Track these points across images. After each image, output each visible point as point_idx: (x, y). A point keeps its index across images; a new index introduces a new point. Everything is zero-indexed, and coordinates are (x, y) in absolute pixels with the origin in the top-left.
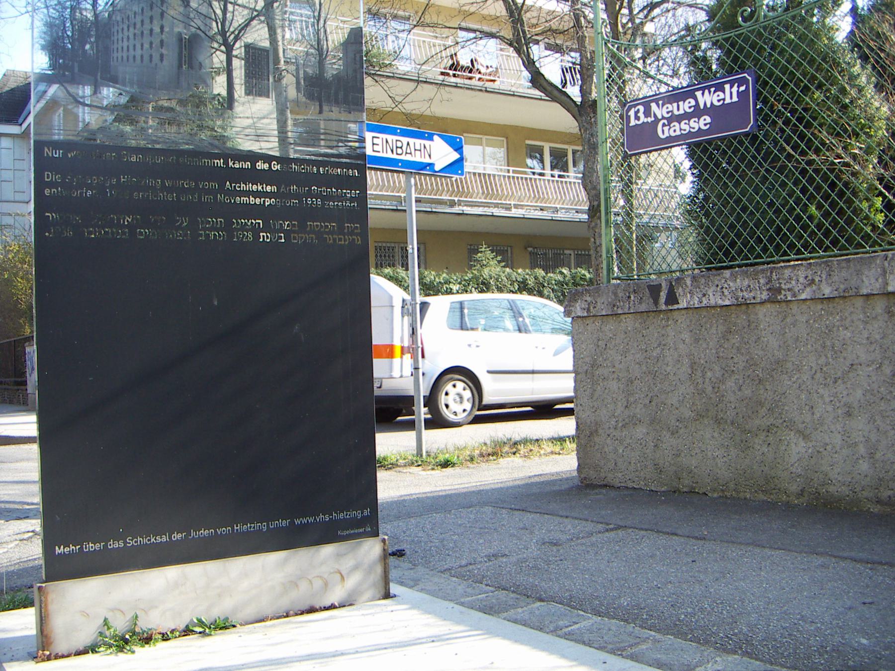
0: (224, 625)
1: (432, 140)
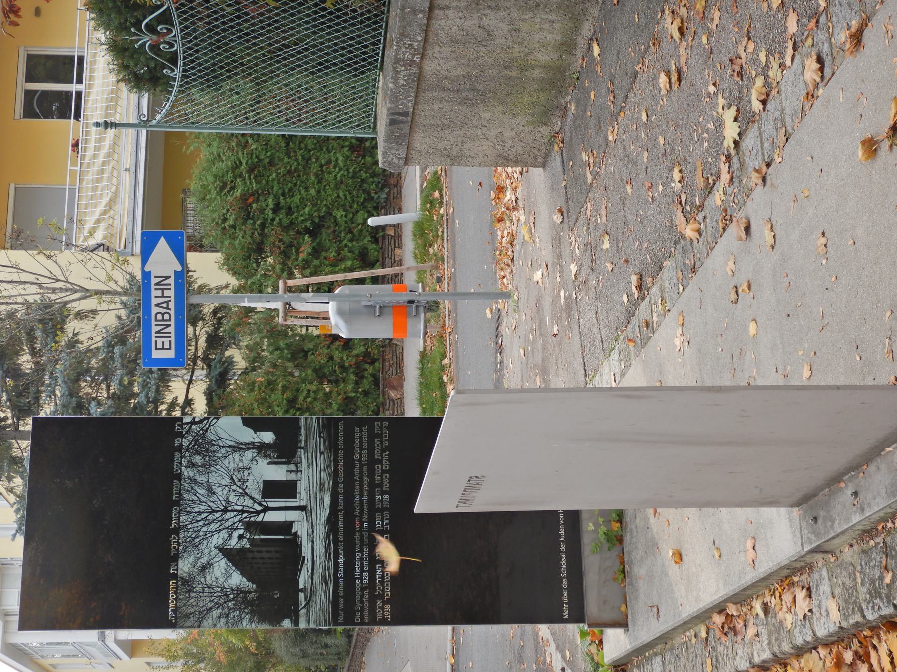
0: (317, 318)
1: (150, 272)
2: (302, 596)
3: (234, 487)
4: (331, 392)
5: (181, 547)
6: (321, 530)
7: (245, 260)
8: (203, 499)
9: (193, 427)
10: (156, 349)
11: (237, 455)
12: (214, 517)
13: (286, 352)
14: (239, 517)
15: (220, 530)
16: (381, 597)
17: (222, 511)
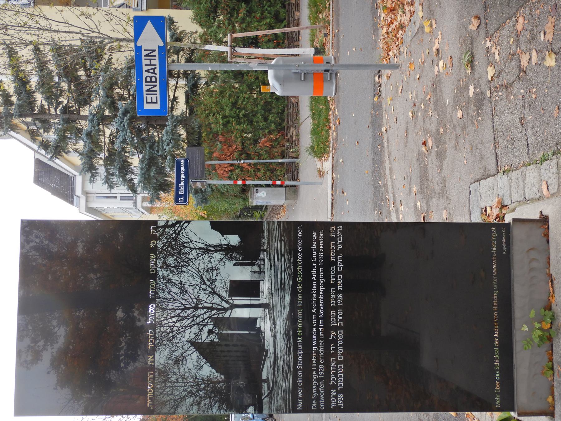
2: (265, 385)
3: (204, 286)
4: (257, 98)
5: (157, 341)
6: (281, 326)
7: (207, 17)
8: (176, 297)
9: (167, 230)
10: (147, 103)
11: (207, 257)
12: (186, 314)
13: (231, 74)
14: (208, 314)
15: (191, 326)
16: (335, 387)
17: (193, 308)
